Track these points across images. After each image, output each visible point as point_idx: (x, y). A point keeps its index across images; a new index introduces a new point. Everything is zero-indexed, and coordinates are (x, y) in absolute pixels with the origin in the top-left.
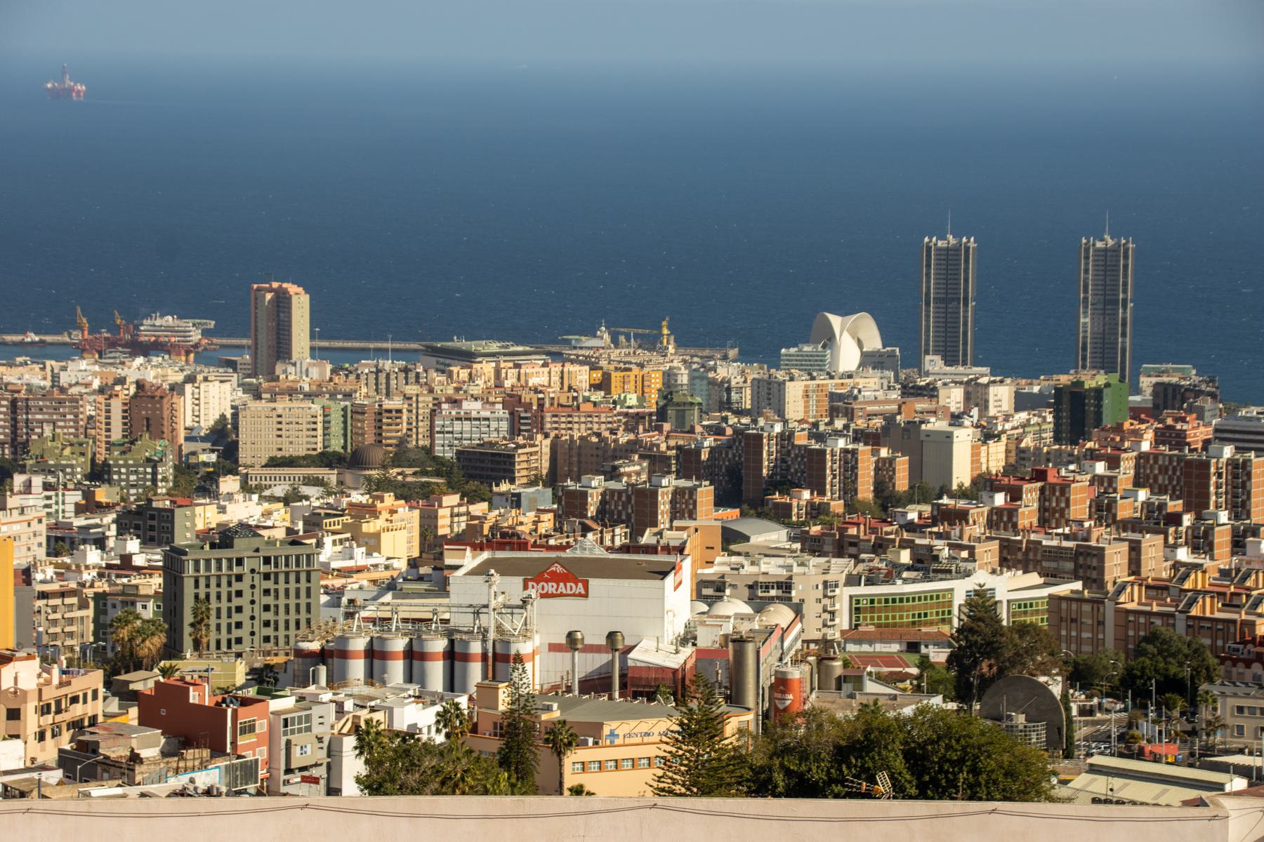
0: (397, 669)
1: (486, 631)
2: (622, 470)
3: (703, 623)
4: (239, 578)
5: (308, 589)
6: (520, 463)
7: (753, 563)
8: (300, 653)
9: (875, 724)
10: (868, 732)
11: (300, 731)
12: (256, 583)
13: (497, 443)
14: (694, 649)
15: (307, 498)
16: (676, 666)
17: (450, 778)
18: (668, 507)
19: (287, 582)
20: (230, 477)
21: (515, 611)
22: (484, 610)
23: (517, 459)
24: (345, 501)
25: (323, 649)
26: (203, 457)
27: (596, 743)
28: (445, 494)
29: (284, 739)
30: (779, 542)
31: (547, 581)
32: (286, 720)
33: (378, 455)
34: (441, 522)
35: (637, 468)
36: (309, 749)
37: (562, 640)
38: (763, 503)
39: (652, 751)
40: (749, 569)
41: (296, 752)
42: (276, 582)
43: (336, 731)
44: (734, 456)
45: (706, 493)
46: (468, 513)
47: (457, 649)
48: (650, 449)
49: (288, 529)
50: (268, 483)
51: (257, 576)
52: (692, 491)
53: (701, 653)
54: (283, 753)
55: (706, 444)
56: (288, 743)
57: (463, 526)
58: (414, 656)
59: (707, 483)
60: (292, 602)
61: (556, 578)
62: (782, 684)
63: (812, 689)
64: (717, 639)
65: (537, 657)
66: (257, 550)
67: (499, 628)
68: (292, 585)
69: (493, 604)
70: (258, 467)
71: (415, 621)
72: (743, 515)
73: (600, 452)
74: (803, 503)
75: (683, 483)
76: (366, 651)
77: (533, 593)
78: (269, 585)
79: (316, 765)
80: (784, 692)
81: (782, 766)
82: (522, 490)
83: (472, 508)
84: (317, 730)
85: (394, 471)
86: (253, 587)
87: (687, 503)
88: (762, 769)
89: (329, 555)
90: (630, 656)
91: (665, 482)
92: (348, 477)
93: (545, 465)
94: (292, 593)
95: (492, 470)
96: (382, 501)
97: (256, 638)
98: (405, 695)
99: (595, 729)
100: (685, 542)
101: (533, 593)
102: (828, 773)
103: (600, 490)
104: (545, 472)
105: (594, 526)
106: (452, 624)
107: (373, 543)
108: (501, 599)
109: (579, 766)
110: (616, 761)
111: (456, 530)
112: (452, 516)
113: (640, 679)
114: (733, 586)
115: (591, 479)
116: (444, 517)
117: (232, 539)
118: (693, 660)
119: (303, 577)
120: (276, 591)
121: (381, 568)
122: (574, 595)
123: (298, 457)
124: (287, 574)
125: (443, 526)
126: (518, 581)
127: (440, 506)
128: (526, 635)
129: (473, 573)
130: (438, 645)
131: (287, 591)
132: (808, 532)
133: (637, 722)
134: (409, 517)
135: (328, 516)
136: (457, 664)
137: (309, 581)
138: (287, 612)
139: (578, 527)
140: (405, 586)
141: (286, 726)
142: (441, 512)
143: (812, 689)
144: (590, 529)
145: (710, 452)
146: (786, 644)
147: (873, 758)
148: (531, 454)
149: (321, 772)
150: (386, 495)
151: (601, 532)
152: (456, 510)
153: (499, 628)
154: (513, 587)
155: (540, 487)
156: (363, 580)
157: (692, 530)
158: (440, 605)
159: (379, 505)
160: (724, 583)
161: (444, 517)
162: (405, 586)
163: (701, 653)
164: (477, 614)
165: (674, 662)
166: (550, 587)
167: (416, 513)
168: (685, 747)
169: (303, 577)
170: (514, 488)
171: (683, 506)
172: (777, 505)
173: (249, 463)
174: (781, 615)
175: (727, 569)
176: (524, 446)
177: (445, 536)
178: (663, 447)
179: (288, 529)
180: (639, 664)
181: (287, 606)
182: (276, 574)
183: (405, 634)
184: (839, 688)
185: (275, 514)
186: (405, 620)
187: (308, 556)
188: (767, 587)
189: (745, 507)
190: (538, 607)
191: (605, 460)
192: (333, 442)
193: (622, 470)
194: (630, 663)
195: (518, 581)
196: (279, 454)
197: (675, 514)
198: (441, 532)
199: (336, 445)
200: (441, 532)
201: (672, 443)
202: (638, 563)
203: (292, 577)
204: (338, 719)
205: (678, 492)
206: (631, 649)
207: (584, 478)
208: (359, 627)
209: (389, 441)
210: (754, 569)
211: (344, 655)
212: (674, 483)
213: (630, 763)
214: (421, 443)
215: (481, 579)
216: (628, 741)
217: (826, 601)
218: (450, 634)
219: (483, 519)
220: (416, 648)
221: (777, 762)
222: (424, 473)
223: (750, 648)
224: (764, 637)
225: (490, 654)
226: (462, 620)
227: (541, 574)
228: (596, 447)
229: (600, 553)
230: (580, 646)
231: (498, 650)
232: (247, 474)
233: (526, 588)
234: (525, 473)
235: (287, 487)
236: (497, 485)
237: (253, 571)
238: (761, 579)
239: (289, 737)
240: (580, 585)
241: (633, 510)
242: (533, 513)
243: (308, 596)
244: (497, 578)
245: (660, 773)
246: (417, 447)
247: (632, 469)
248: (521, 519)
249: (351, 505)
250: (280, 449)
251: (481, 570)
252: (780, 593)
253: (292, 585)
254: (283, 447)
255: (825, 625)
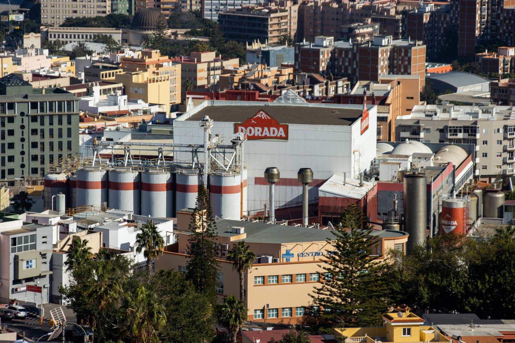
0: (128, 198)
1: (203, 167)
2: (357, 31)
3: (385, 162)
4: (11, 120)
5: (69, 130)
6: (272, 25)
7: (444, 111)
8: (48, 183)
9: (506, 247)
10: (500, 253)
11: (26, 248)
12: (26, 124)
13: (253, 8)
14: (376, 183)
15: (90, 53)
16: (359, 197)
17: (96, 292)
18: (386, 63)
19: (51, 124)
20: (32, 35)
21: (227, 150)
22: (201, 149)
23: (270, 22)
24: (120, 55)
25: (68, 180)
26: (13, 17)
27: (274, 261)
28: (203, 51)
29: (12, 256)
30: (482, 92)
31: (254, 126)
32: (14, 239)
33: (154, 17)
34: (199, 75)
35: (370, 30)
36: (34, 264)
37: (262, 175)
38: (475, 59)
39: (313, 268)
40: (441, 116)
41: (23, 266)
42: (42, 124)
43: (58, 249)
44: (451, 19)
45: (419, 50)
46: (222, 68)
47: (178, 181)
48: (382, 14)
49: (72, 79)
50: (65, 40)
51: (26, 119)
52: (407, 49)
53: (383, 188)
54: (12, 267)
55: (428, 9)
56: (16, 258)
57: (218, 78)
58: (143, 187)
59: (421, 42)
60: (56, 140)
61: (262, 123)
62: (448, 211)
63: (478, 217)
64: (396, 175)
65: (245, 190)
66: (26, 97)
67: (213, 164)
68: (56, 127)
69: (208, 144)
70: (56, 26)
71: (144, 158)
72: (455, 69)
73: (340, 17)
74: (509, 59)
75: (400, 43)
76: (102, 182)
77: (241, 135)
78: (36, 125)
79: (40, 277)
80: (449, 220)
81: (426, 281)
82: (271, 48)
83: (225, 63)
84: (41, 248)
85: (169, 32)
86: (23, 127)
87: (403, 60)
88: (410, 284)
89: (97, 101)
90: (321, 188)
91: (384, 42)
92: (132, 36)
93: (294, 26)
94: (56, 133)
95: (249, 31)
96: (150, 57)
97: (26, 170)
98: (121, 219)
99: (274, 250)
100: (389, 92)
101: (241, 135)
102: (466, 288)
103: (330, 49)
104: (293, 33)
105: (321, 79)
106: (175, 161)
107: (136, 93)
108: (215, 140)
109: (260, 279)
110: (291, 276)
111: (212, 81)
112: (209, 70)
113: (329, 207)
114: (427, 130)
115: (323, 40)
116: (202, 70)
117: (5, 87)
118: (375, 192)
119: (65, 120)
120: (42, 131)
121: (140, 113)
122: (276, 138)
123: (90, 19)
124: (51, 117)
125: (201, 79)
126: (230, 125)
127: (199, 61)
128: (235, 170)
129: (194, 118)
130: (162, 178)
131: (51, 131)
132: (497, 84)
133: (309, 244)
134: (173, 70)
135: (105, 68)
136: (178, 194)
137: (69, 123)
138: (52, 149)
139: (307, 79)
140: (154, 128)
141: (14, 244)
142: (199, 66)
143: (478, 217)
144: (317, 82)
145: (431, 16)
146: (457, 179)
147: (504, 275)
148: (282, 18)
149: (44, 282)
150: (154, 52)
151: (327, 84)
152: (212, 65)
153: (213, 164)
154: (226, 131)
155: (286, 46)
156: (125, 123)
157: (395, 83)
158: (165, 145)
159: (147, 60)
160: (419, 127)
161: (202, 70)
162: (154, 128)
163: (383, 188)
164: (195, 152)
165: (358, 194)
166: (257, 131)
167: (179, 67)
168: (340, 265)
169: (65, 120)
170: (265, 47)
171: (400, 63)
172: (486, 61)
173: (49, 23)
174: (455, 155)
175: (422, 116)
176: (275, 11)
177: (203, 86)
178: (393, 12)
179: (72, 79)
180: (328, 195)
181: (51, 144)
182: (42, 117)
183: (135, 169)
184: (501, 216)
185: (63, 66)
186: (136, 157)
187: (69, 103)
188: (455, 131)
189: (456, 62)
190: (246, 147)
191: (344, 23)
192: (120, 6)
193: (357, 31)
194: (321, 194)
195: (230, 125)
196: (75, 16)
197: (392, 69)
198: (199, 83)
199: (123, 8)
200: (199, 83)
201: (400, 8)
202: (332, 111)
203: (56, 120)
204: (61, 238)
205: (395, 50)
206: (323, 182)
207: (318, 38)
208: (97, 162)
209: (165, 6)
210: (446, 116)
211: (85, 185)
212: (393, 43)
213: (303, 277)
214: (194, 8)
215: (197, 123)
216: (301, 259)
217: (506, 143)
218: (172, 169)
219: (233, 72)
220: (144, 181)
221: (422, 278)
222: (193, 33)
223: (421, 183)
224: (437, 173)
225: (205, 186)
226: (183, 158)
227: (249, 120)
228: (337, 12)
229: (301, 102)
230: (276, 180)
231: (212, 183)
232: (47, 32)
233: (236, 131)
234: (276, 34)
235: (76, 44)
236: (250, 44)
237: (22, 114)
238: (450, 124)
239: (17, 253)
240: (281, 129)
241: (360, 64)
242: (276, 68)
243: (69, 135)
244: (211, 123)
245: (319, 286)
246: (191, 11)
247: (365, 30)
248: (266, 73)
249: (124, 59)
250: (75, 12)
251: (199, 117)
252: (466, 136)
253: (56, 127)
254: (78, 9)
255: (505, 163)
